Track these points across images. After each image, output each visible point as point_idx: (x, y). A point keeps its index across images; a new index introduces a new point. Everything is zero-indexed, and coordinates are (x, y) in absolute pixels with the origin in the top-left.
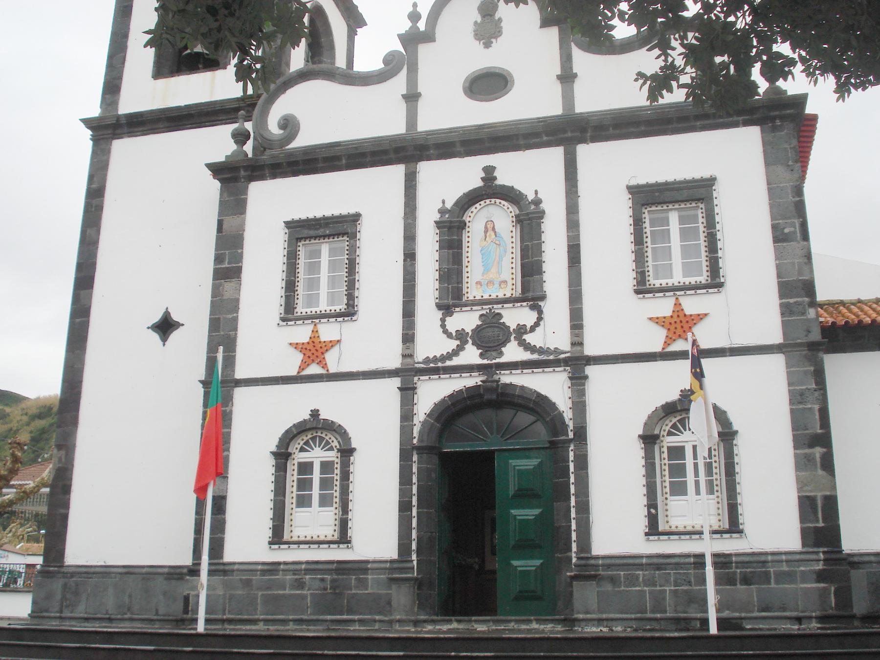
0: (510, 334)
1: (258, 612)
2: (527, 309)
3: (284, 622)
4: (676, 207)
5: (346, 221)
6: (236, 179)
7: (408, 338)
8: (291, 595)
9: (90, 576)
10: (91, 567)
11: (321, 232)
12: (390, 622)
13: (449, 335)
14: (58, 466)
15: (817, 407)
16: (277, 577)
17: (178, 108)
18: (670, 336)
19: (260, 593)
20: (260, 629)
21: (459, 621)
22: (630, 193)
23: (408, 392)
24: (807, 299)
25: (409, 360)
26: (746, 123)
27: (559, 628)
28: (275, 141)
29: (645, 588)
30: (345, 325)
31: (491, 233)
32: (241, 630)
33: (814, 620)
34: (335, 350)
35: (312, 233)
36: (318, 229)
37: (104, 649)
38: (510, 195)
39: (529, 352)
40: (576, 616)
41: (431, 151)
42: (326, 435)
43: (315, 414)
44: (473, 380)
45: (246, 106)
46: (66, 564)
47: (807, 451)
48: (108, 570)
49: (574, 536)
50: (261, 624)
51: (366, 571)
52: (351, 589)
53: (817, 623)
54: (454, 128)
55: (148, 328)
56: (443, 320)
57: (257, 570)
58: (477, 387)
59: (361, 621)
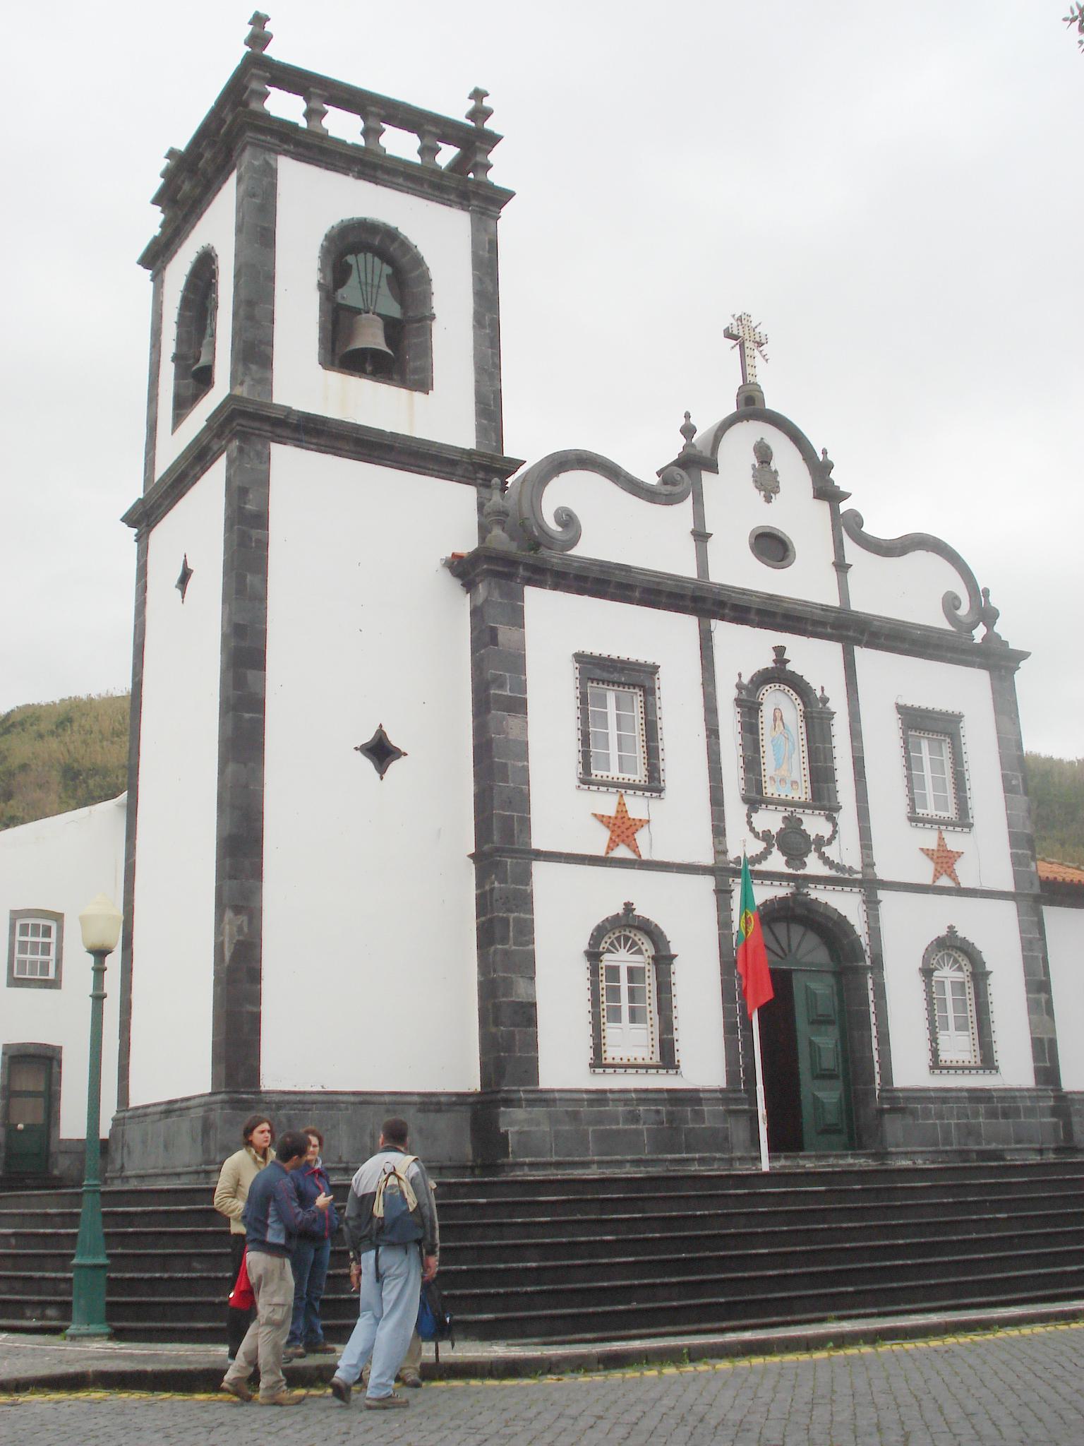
0: (811, 844)
1: (591, 1153)
2: (823, 819)
3: (620, 1163)
4: (935, 737)
5: (644, 672)
6: (509, 576)
7: (719, 831)
8: (626, 1131)
9: (307, 1106)
10: (304, 1093)
11: (615, 677)
12: (730, 1161)
13: (756, 835)
14: (237, 938)
15: (1041, 955)
16: (607, 1108)
17: (381, 433)
18: (611, 821)
19: (591, 1129)
20: (593, 1173)
21: (786, 1158)
22: (899, 713)
23: (723, 894)
24: (1029, 852)
25: (722, 857)
26: (981, 667)
27: (871, 1162)
28: (557, 540)
29: (937, 1121)
30: (652, 802)
31: (779, 722)
32: (572, 1174)
33: (1051, 1151)
34: (645, 830)
35: (605, 675)
36: (612, 673)
37: (774, 1194)
38: (797, 685)
39: (828, 867)
40: (889, 1149)
41: (727, 611)
42: (635, 935)
43: (629, 907)
44: (781, 891)
45: (467, 463)
46: (263, 1088)
47: (1036, 996)
48: (334, 1098)
49: (877, 1068)
50: (595, 1167)
51: (699, 1101)
52: (688, 1123)
53: (1054, 1154)
54: (777, 596)
55: (356, 749)
56: (749, 816)
57: (583, 1100)
58: (783, 900)
59: (702, 1161)
